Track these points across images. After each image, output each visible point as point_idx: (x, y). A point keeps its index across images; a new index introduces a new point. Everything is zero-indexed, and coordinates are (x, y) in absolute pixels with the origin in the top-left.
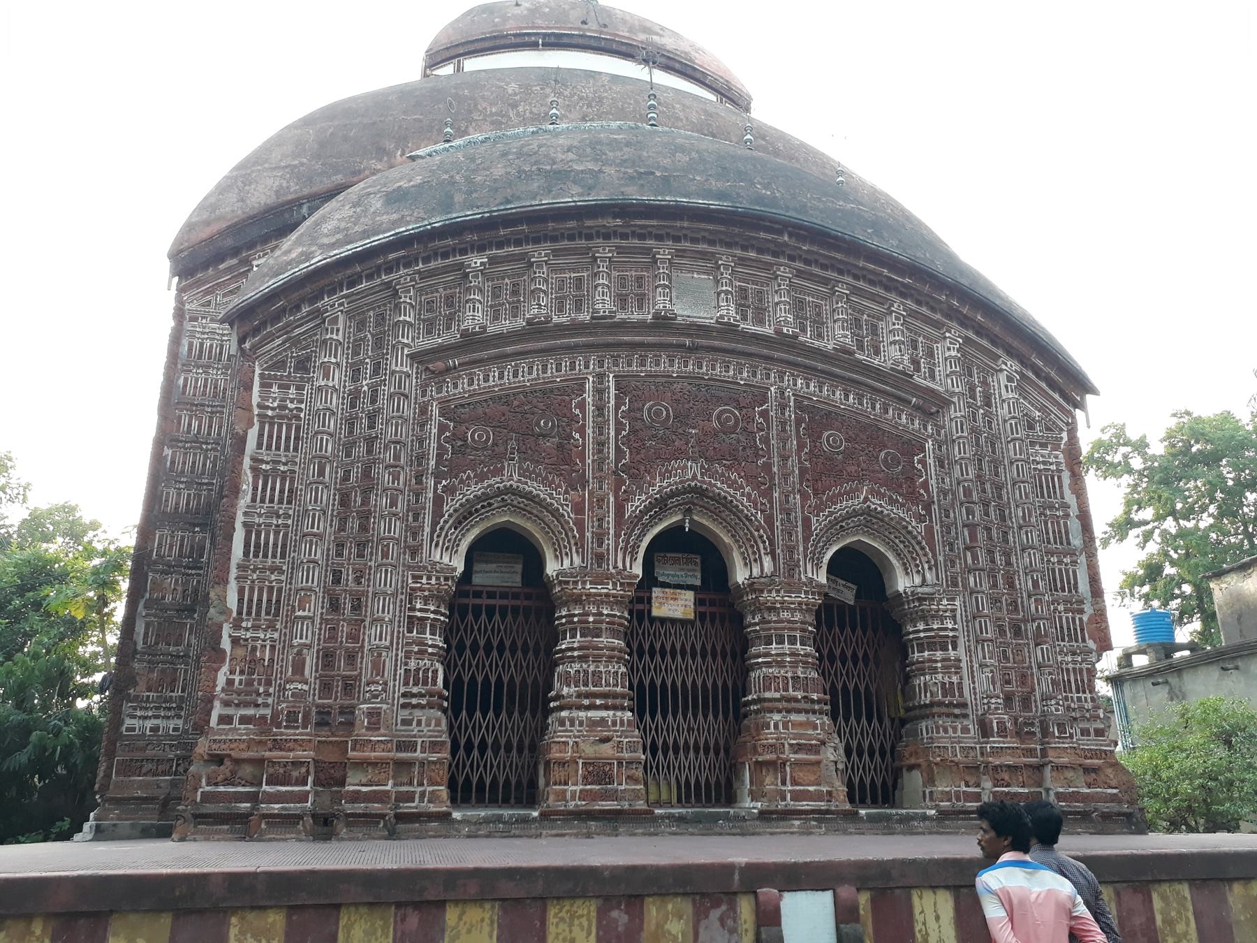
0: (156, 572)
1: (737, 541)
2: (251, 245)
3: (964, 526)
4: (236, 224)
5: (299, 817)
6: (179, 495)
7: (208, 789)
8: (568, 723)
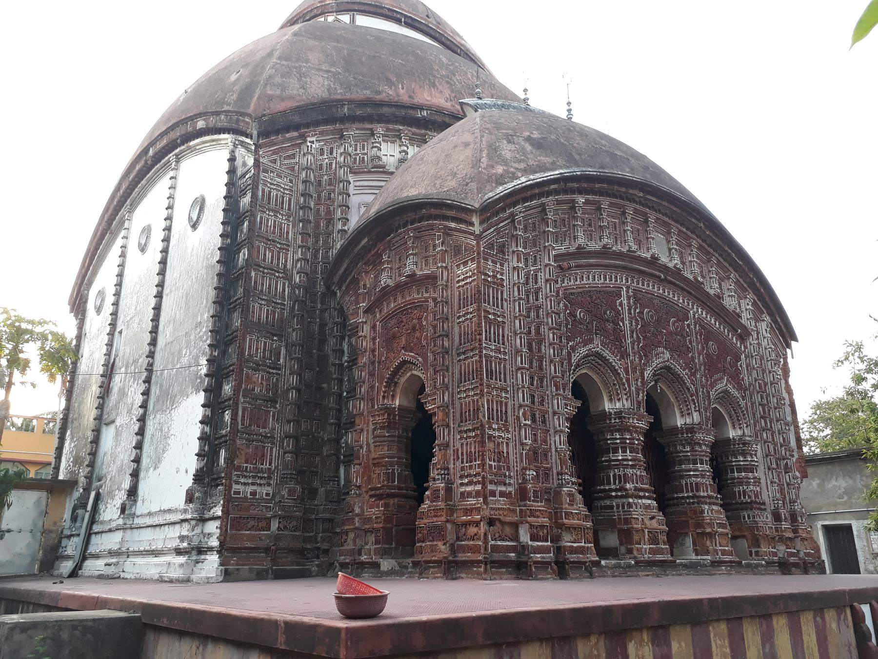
0: (249, 368)
2: (307, 125)
3: (760, 405)
4: (303, 106)
5: (549, 563)
6: (261, 309)
7: (493, 542)
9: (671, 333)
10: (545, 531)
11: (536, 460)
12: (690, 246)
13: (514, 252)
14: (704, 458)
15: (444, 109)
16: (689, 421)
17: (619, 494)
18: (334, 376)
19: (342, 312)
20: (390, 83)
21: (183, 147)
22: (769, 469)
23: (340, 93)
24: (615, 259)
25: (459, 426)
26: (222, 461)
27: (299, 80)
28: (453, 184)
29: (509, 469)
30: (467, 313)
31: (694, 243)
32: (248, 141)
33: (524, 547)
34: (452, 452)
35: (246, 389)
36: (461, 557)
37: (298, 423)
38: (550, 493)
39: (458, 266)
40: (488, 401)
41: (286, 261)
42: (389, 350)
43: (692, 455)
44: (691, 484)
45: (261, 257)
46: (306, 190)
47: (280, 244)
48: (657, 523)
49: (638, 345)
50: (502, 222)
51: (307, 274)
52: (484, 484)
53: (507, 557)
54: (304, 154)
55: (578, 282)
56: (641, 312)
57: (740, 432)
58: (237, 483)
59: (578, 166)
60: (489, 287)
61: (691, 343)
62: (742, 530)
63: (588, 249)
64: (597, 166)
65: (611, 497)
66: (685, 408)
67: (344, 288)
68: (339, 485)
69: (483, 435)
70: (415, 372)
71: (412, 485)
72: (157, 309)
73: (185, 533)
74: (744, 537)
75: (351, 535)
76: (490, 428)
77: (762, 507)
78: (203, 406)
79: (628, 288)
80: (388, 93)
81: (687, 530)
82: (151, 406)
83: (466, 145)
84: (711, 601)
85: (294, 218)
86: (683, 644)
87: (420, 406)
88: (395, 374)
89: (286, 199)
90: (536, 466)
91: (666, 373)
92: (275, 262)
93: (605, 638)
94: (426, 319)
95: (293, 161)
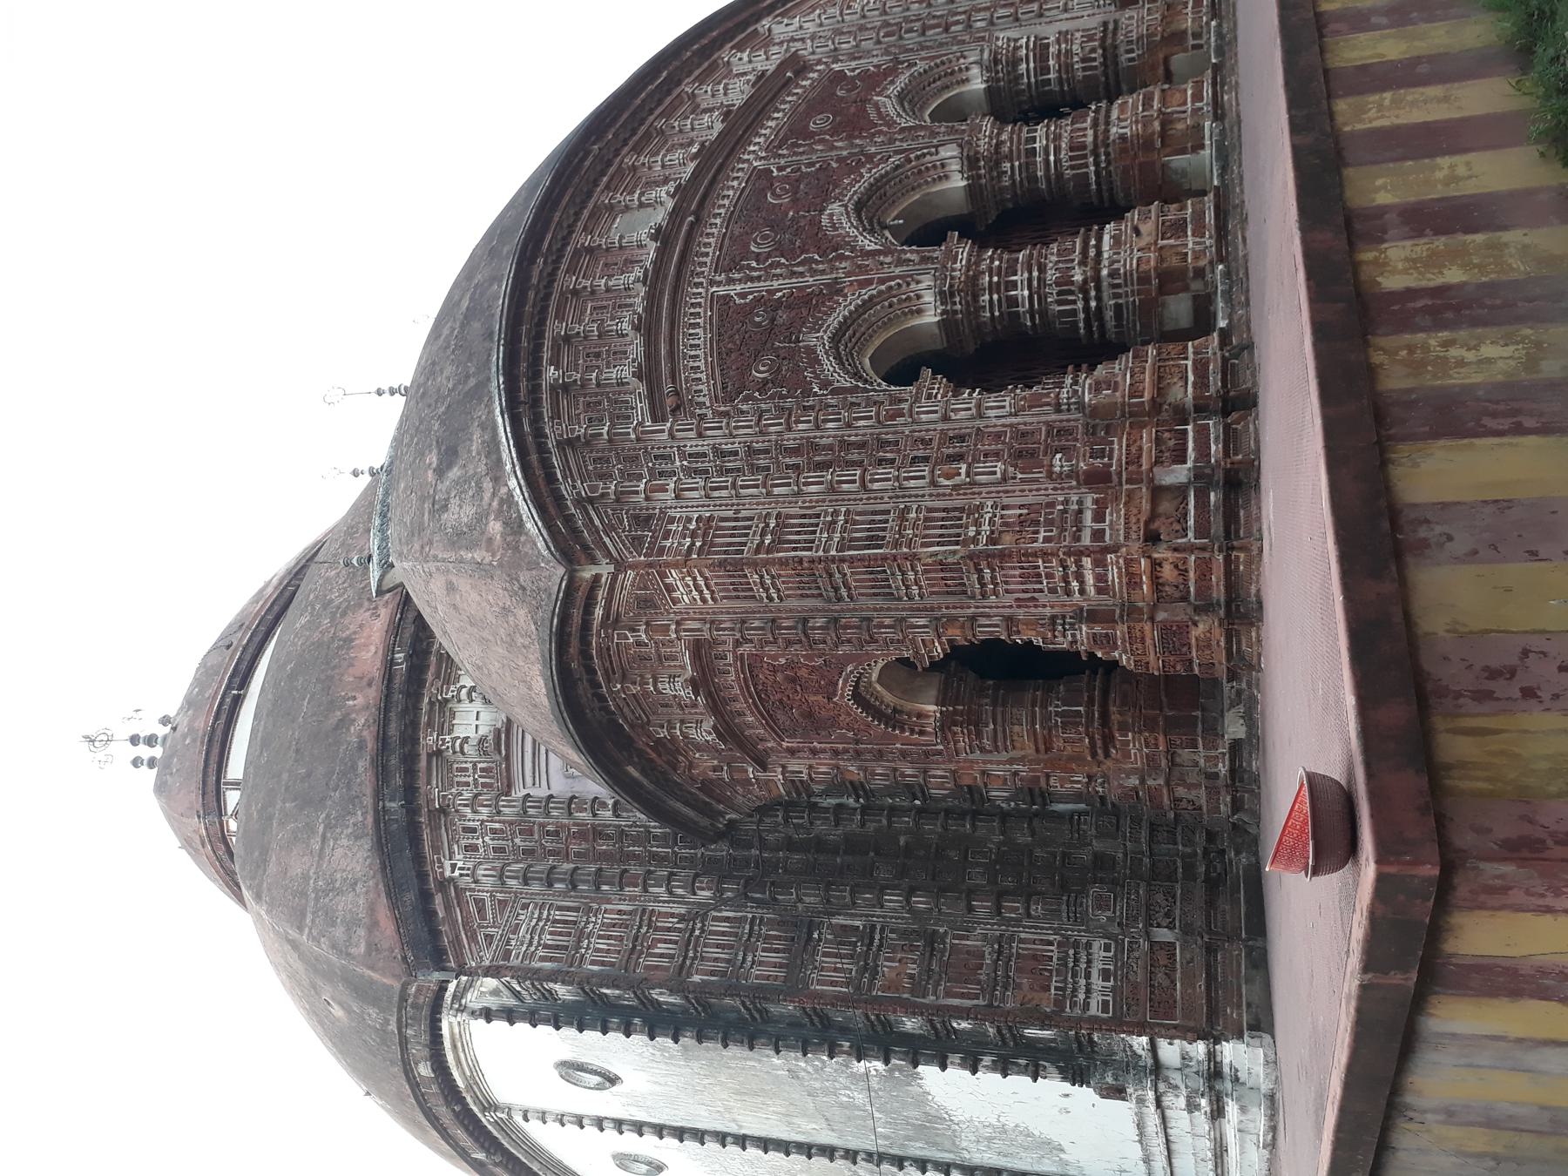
1: (919, 186)
2: (422, 877)
3: (923, 34)
4: (387, 886)
5: (1227, 427)
6: (761, 963)
7: (1191, 534)
8: (1116, 266)
9: (795, 201)
10: (1167, 435)
11: (1033, 454)
12: (634, 168)
13: (647, 499)
14: (1024, 135)
15: (392, 621)
16: (955, 166)
17: (1093, 293)
18: (885, 822)
19: (764, 810)
20: (345, 722)
21: (469, 1100)
22: (1041, 15)
23: (363, 817)
24: (660, 307)
25: (973, 597)
26: (1046, 1034)
27: (340, 892)
28: (522, 613)
29: (1051, 505)
30: (762, 584)
31: (629, 161)
32: (452, 987)
33: (1198, 475)
34: (1021, 611)
35: (912, 992)
36: (1219, 593)
37: (971, 893)
38: (1094, 427)
39: (675, 601)
40: (924, 545)
41: (672, 915)
42: (834, 722)
43: (1019, 158)
44: (1071, 159)
45: (665, 962)
46: (540, 879)
47: (640, 927)
48: (1146, 222)
49: (817, 262)
50: (591, 520)
51: (697, 875)
52: (1080, 553)
53: (1217, 509)
54: (476, 882)
55: (703, 376)
56: (757, 257)
57: (975, 70)
58: (1086, 1006)
59: (489, 379)
60: (712, 545)
61: (812, 164)
62: (1155, 65)
63: (641, 358)
64: (487, 344)
65: (1099, 308)
66: (932, 172)
67: (721, 807)
68: (1086, 813)
69: (988, 555)
70: (875, 676)
71: (1085, 677)
72: (766, 1144)
73: (1182, 1102)
74: (1166, 60)
75: (1181, 791)
76: (975, 540)
77: (1111, 27)
78: (944, 1067)
79: (712, 283)
80: (362, 726)
81: (1158, 166)
82: (947, 1157)
83: (451, 588)
84: (1295, 128)
85: (593, 900)
86: (1379, 182)
87: (935, 666)
88: (878, 714)
89: (558, 915)
90: (1045, 454)
91: (868, 210)
92: (674, 936)
93: (1374, 334)
94: (775, 658)
95: (488, 904)
